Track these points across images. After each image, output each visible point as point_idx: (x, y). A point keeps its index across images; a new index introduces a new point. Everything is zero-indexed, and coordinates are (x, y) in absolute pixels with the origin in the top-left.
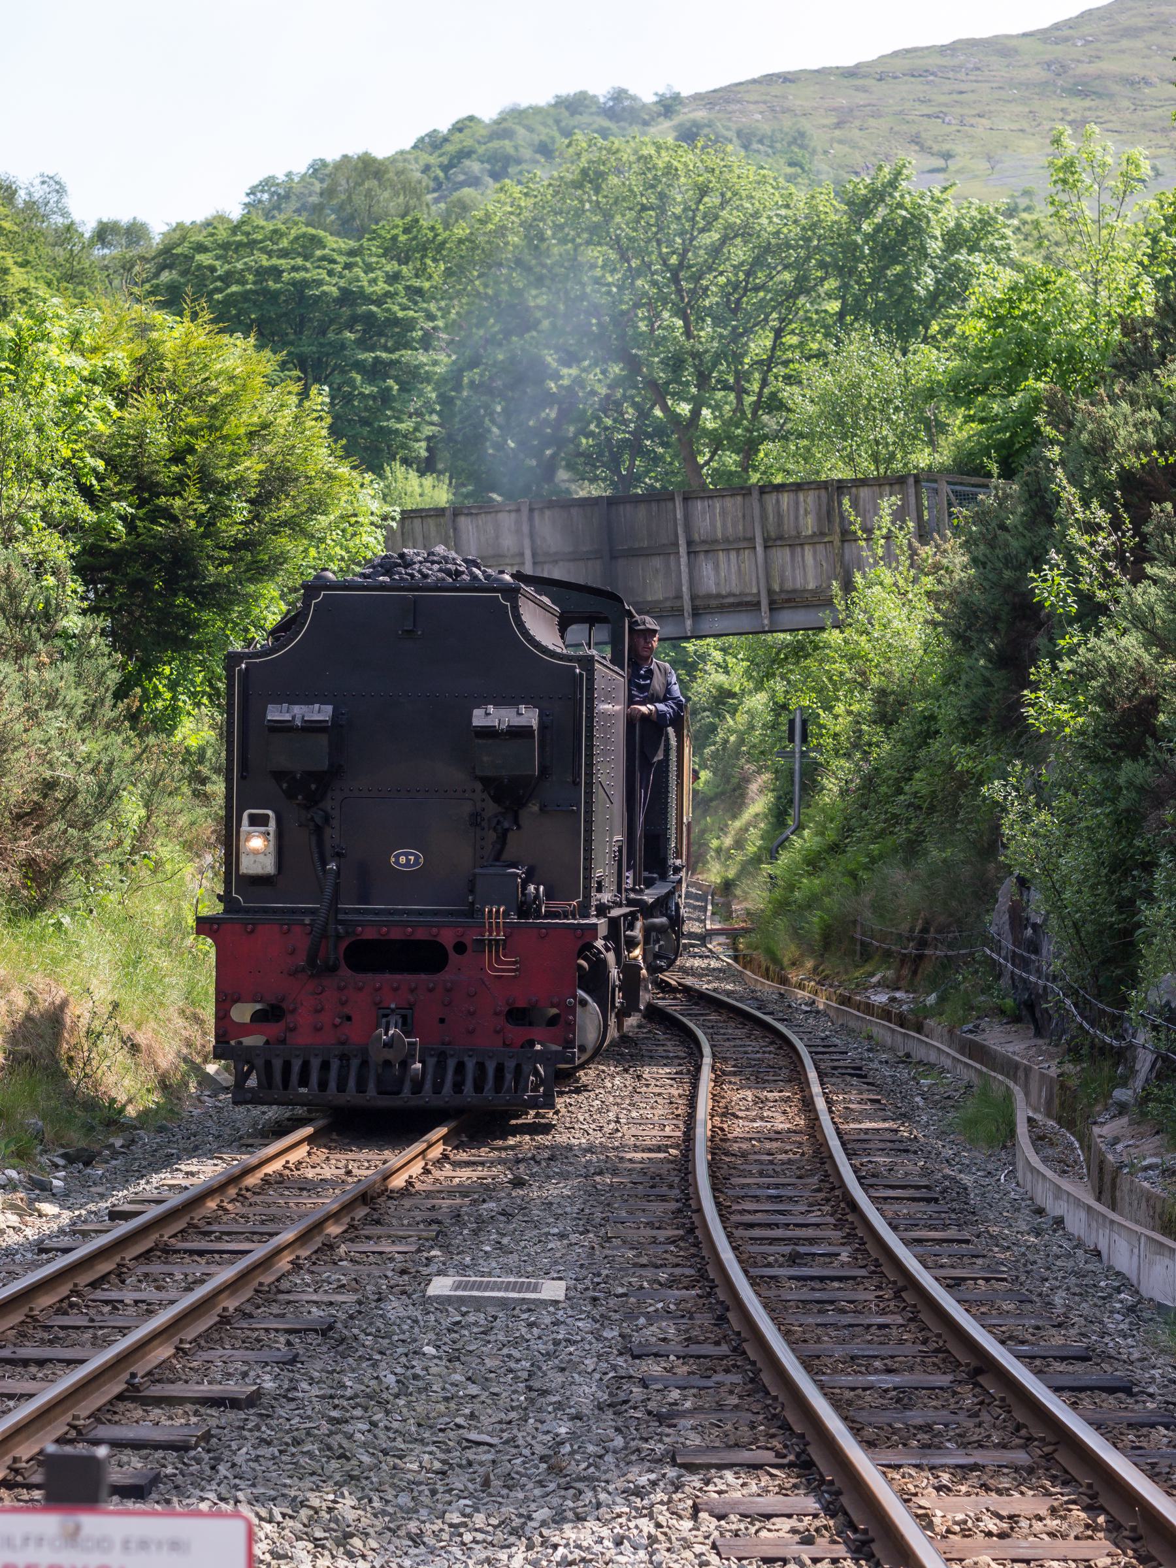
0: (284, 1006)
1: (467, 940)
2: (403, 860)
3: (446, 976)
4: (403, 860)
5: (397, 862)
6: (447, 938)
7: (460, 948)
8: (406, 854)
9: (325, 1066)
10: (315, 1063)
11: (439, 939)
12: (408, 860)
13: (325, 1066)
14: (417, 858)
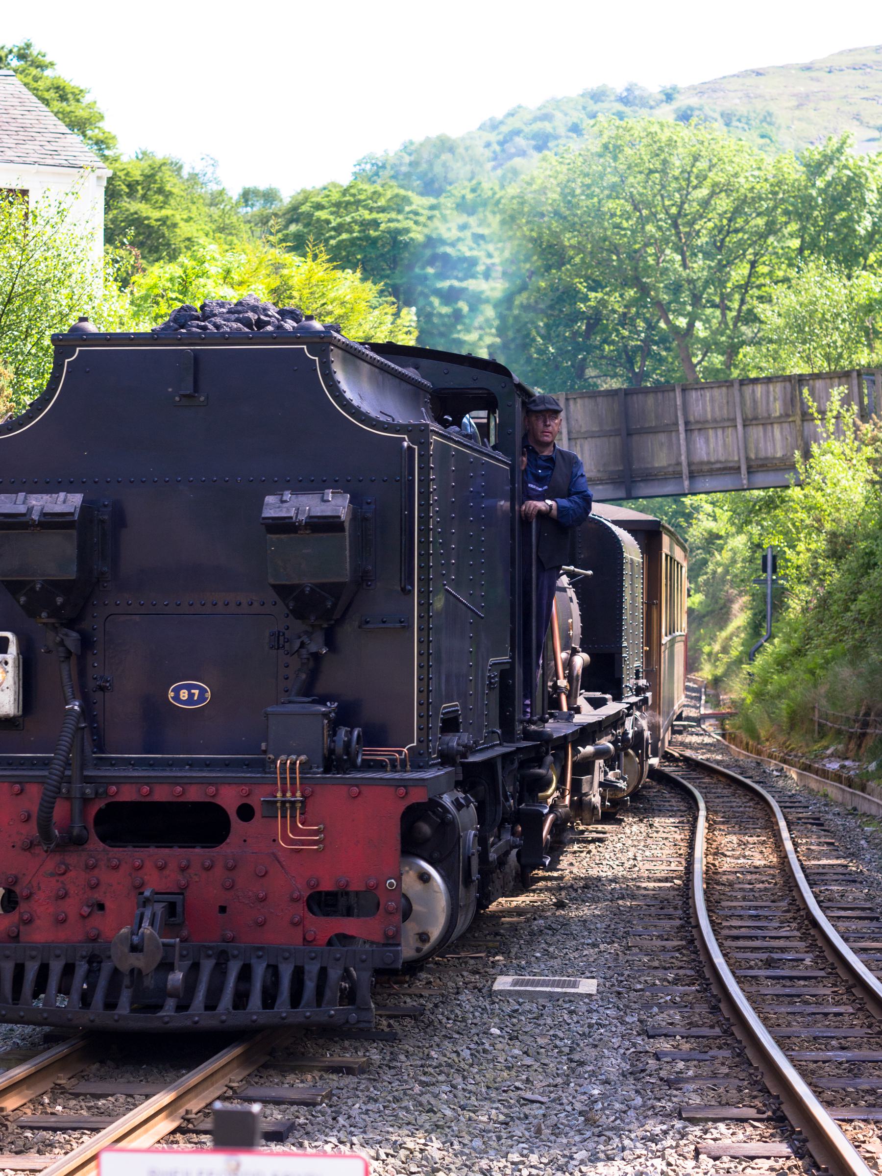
2: (184, 695)
4: (184, 695)
5: (177, 698)
7: (246, 812)
8: (189, 687)
11: (218, 801)
12: (191, 695)
13: (69, 970)
14: (202, 691)
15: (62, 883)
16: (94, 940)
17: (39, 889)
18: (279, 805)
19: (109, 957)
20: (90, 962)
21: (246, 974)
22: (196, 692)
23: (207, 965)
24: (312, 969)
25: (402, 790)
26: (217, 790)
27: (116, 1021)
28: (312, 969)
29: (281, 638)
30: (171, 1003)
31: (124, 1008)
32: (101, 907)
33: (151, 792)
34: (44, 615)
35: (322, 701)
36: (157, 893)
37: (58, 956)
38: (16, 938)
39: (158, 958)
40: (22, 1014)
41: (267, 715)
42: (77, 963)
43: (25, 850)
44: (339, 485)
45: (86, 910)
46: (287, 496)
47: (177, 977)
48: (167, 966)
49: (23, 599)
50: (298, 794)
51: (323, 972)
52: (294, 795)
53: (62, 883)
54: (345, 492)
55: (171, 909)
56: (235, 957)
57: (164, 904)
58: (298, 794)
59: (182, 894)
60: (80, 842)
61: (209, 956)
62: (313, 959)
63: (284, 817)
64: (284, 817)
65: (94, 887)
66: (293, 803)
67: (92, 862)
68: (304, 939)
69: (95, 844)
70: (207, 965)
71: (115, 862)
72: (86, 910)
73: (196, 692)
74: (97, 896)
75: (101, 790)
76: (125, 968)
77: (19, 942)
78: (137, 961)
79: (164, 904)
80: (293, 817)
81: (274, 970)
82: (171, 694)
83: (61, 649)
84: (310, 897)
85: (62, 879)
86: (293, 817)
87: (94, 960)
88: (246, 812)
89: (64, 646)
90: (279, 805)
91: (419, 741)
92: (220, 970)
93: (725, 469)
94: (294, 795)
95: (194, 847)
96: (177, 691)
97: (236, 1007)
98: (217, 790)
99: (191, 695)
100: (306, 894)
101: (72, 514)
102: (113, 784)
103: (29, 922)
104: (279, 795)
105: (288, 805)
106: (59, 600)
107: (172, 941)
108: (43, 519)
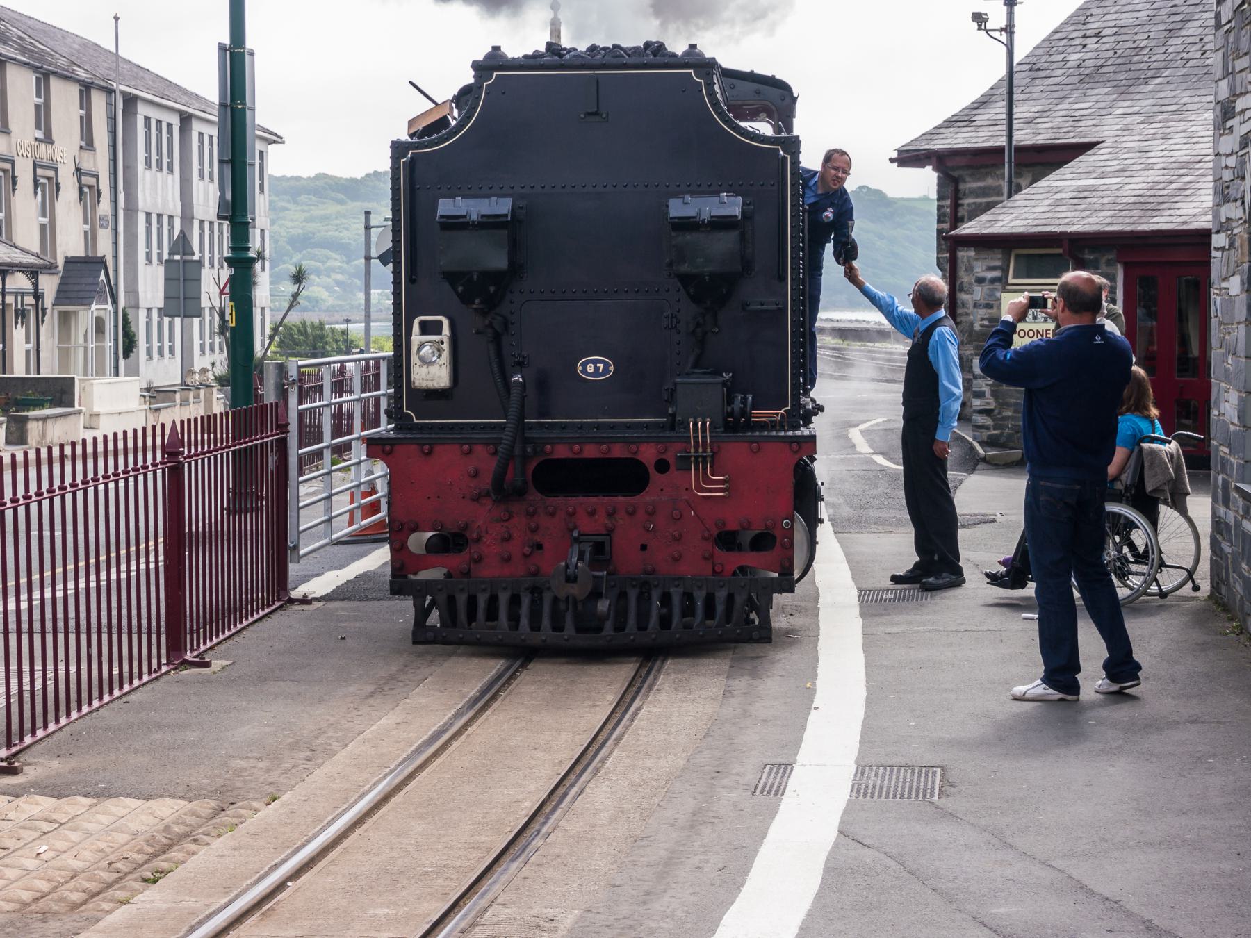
0: (467, 534)
1: (669, 457)
2: (590, 368)
3: (647, 497)
4: (590, 368)
5: (584, 371)
6: (648, 454)
7: (662, 466)
8: (595, 362)
9: (515, 601)
10: (504, 598)
11: (639, 457)
12: (597, 369)
13: (515, 601)
14: (606, 365)
15: (507, 527)
16: (535, 574)
17: (487, 533)
18: (692, 459)
19: (549, 589)
20: (532, 593)
21: (666, 599)
22: (601, 366)
23: (633, 594)
24: (721, 595)
25: (388, 448)
26: (638, 448)
27: (566, 640)
28: (721, 595)
29: (674, 320)
30: (608, 625)
31: (570, 629)
32: (539, 547)
33: (581, 451)
34: (477, 301)
35: (717, 373)
36: (583, 535)
37: (505, 589)
38: (467, 574)
39: (590, 587)
40: (478, 636)
41: (675, 384)
42: (521, 593)
43: (473, 500)
44: (733, 190)
45: (527, 550)
46: (688, 198)
47: (603, 606)
48: (596, 595)
49: (460, 289)
50: (709, 450)
51: (730, 598)
52: (705, 451)
53: (507, 527)
54: (737, 195)
55: (599, 548)
56: (656, 586)
57: (591, 544)
58: (709, 450)
59: (609, 535)
60: (520, 493)
61: (634, 586)
62: (722, 587)
63: (697, 469)
64: (697, 469)
65: (534, 530)
66: (704, 458)
67: (531, 509)
68: (714, 569)
69: (535, 496)
70: (633, 594)
71: (551, 509)
72: (527, 550)
73: (601, 366)
74: (537, 538)
75: (538, 449)
76: (562, 595)
77: (470, 577)
78: (574, 590)
79: (591, 544)
80: (705, 469)
81: (688, 596)
82: (579, 368)
83: (490, 330)
84: (719, 535)
85: (506, 524)
86: (705, 469)
87: (537, 591)
88: (662, 466)
89: (493, 328)
90: (692, 459)
91: (792, 405)
92: (644, 598)
93: (233, 162)
94: (705, 451)
95: (616, 496)
96: (585, 365)
97: (554, 629)
98: (552, 448)
99: (597, 369)
100: (715, 532)
101: (506, 216)
102: (548, 444)
103: (479, 560)
104: (692, 450)
105: (700, 459)
106: (492, 289)
107: (601, 574)
108: (480, 220)
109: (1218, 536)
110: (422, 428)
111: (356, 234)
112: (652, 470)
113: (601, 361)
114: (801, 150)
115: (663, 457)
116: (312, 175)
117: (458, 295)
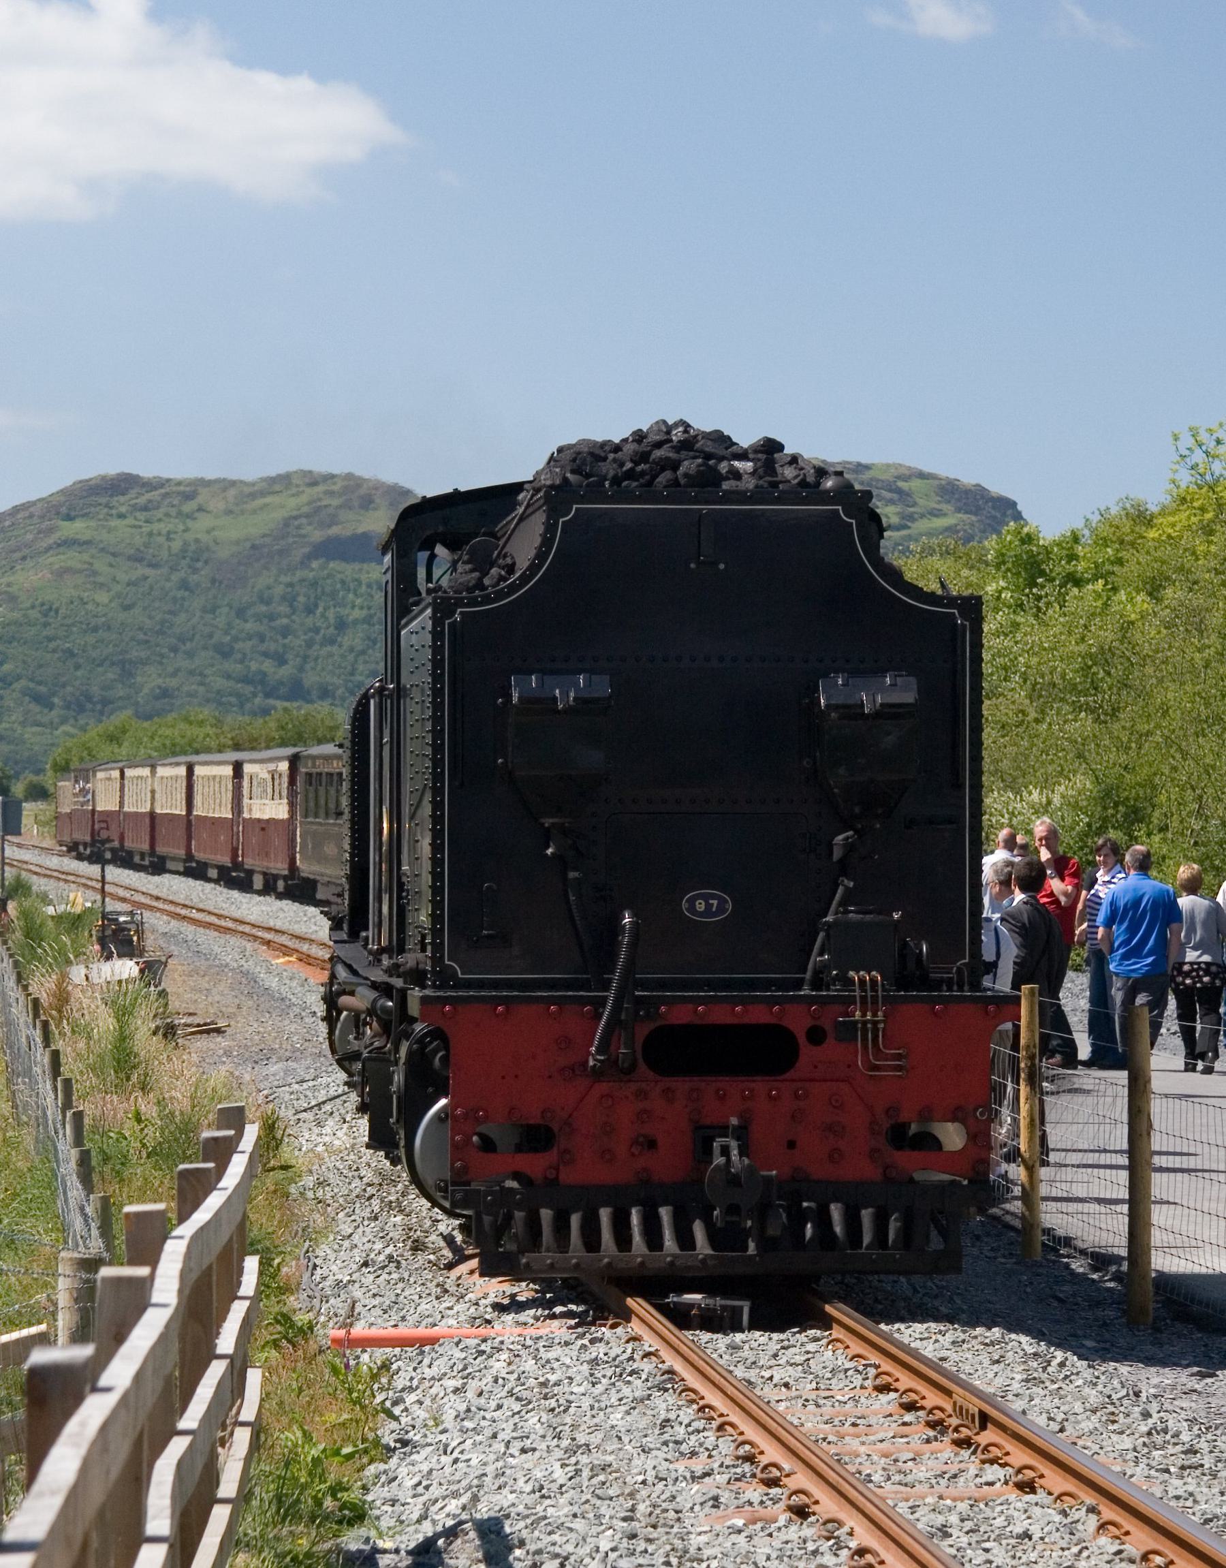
2: (700, 906)
4: (700, 906)
5: (692, 908)
7: (816, 1036)
8: (706, 898)
11: (785, 1023)
12: (709, 906)
14: (722, 902)
22: (715, 902)
73: (715, 902)
96: (692, 902)
99: (709, 906)
109: (672, 1298)
110: (468, 985)
111: (909, 528)
112: (802, 1039)
113: (713, 897)
114: (450, 490)
115: (818, 1023)
116: (708, 429)
117: (216, 881)
